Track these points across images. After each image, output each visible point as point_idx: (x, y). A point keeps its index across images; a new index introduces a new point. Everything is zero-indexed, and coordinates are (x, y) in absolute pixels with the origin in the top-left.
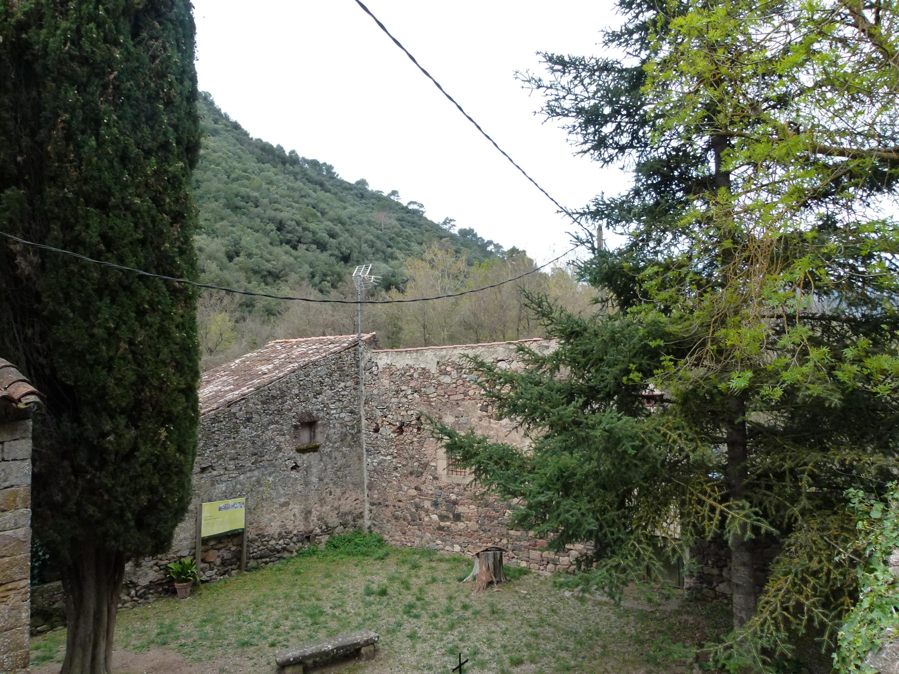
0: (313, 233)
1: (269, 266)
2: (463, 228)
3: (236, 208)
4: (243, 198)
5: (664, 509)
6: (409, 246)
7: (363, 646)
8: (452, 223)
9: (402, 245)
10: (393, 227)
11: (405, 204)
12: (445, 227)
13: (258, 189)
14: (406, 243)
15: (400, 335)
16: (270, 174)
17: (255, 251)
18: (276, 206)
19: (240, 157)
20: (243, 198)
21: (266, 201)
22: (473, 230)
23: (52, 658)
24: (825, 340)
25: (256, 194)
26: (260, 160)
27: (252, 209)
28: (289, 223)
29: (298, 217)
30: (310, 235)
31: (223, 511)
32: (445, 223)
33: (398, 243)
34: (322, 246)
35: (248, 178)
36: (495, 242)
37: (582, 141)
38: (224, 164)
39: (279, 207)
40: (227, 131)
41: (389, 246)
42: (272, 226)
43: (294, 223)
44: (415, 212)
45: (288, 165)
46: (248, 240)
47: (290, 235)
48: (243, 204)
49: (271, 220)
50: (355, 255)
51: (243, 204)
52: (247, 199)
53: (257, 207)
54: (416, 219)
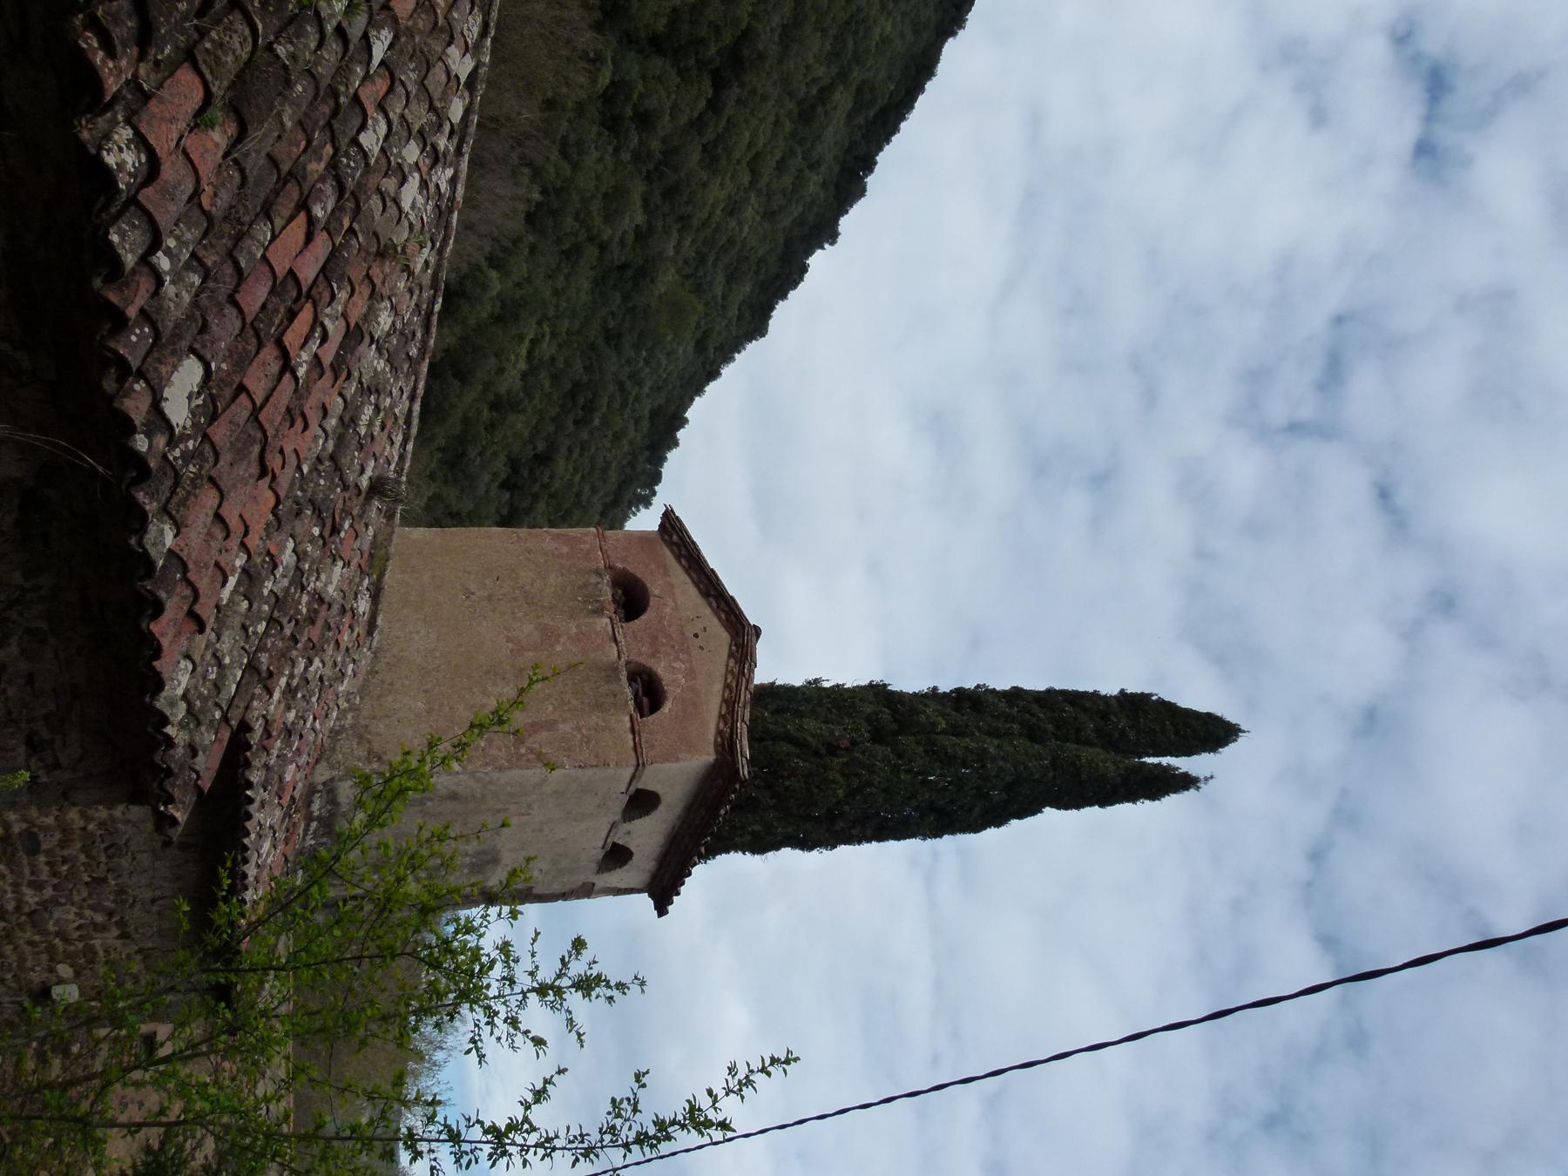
1: (473, 453)
3: (573, 394)
4: (591, 401)
5: (498, 310)
13: (605, 423)
16: (632, 433)
17: (498, 436)
18: (577, 451)
19: (659, 389)
20: (591, 401)
21: (585, 436)
23: (217, 564)
24: (337, 933)
25: (597, 422)
26: (654, 414)
27: (571, 416)
28: (547, 473)
29: (557, 484)
30: (525, 505)
31: (750, 1054)
35: (623, 406)
38: (647, 370)
39: (575, 456)
40: (704, 364)
42: (541, 446)
43: (546, 479)
45: (647, 453)
46: (519, 424)
47: (526, 473)
48: (581, 401)
49: (553, 446)
51: (581, 401)
52: (590, 408)
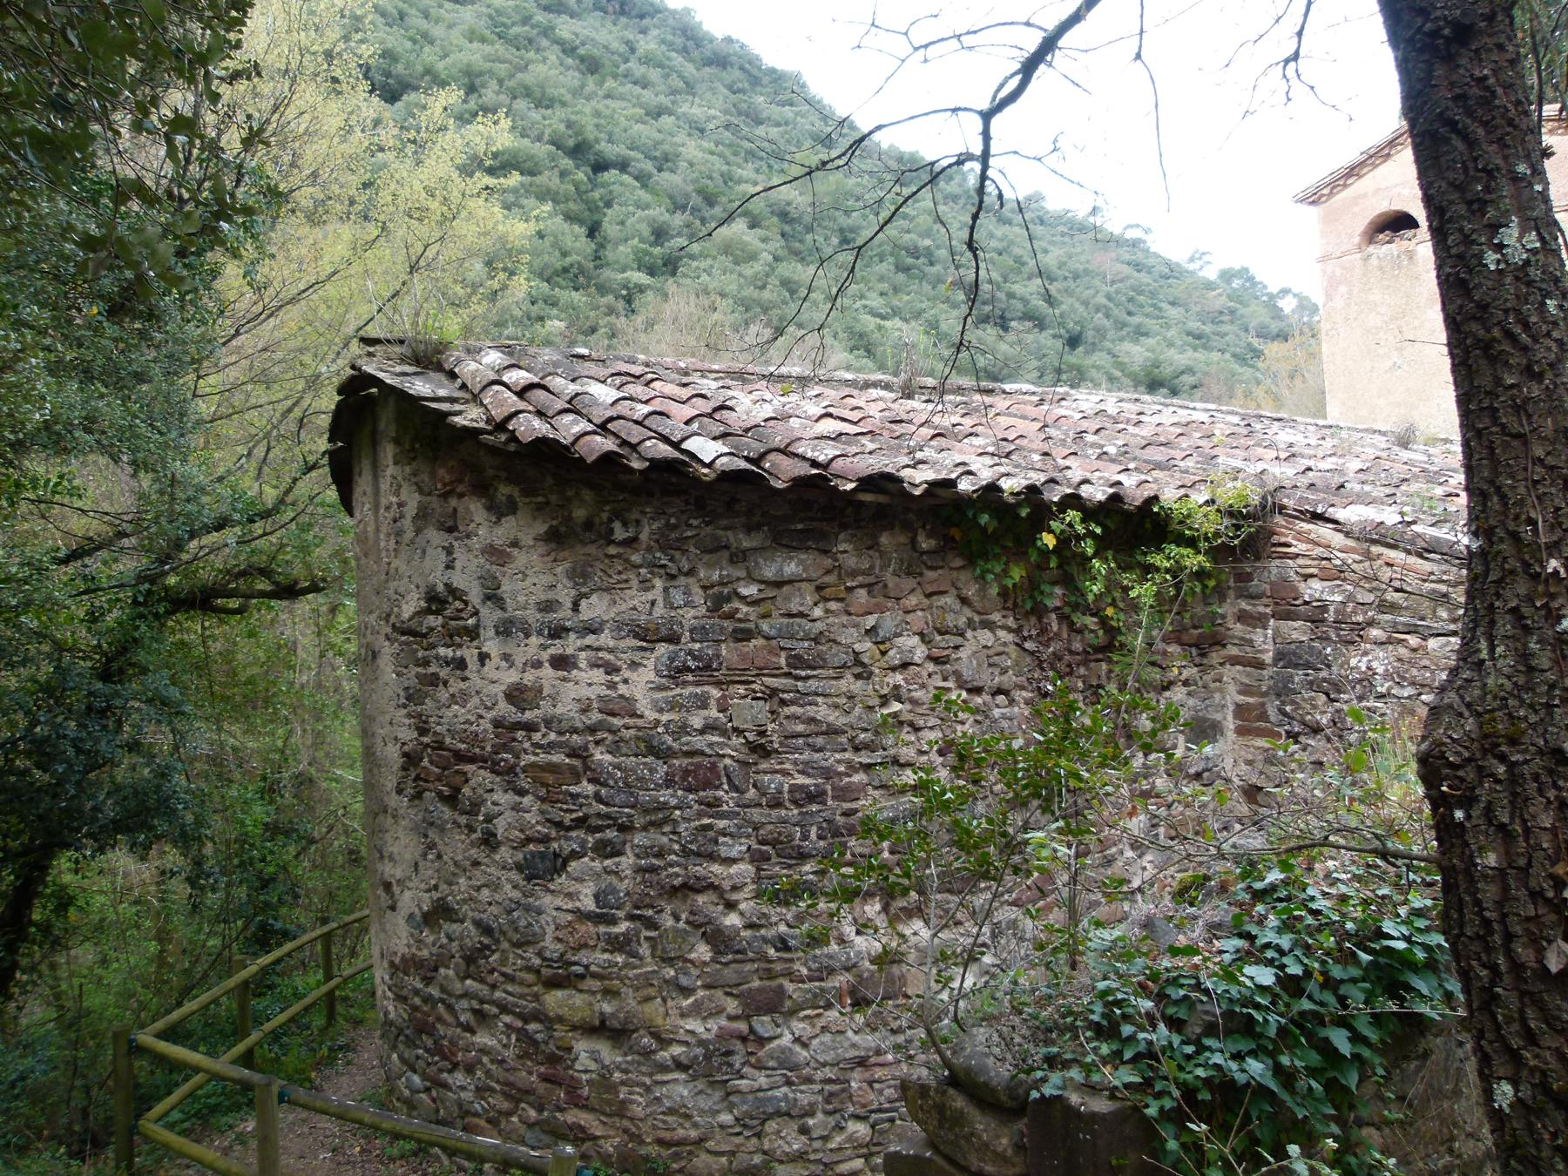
0: (1022, 299)
2: (1227, 266)
6: (1160, 309)
7: (1238, 1031)
8: (1206, 258)
9: (1149, 310)
10: (1128, 278)
11: (1117, 232)
12: (1191, 267)
14: (1154, 305)
15: (423, 604)
22: (1247, 270)
30: (1020, 306)
32: (1192, 260)
33: (1142, 306)
34: (1040, 323)
36: (1295, 290)
37: (768, 333)
41: (1130, 314)
44: (1135, 244)
47: (988, 308)
50: (1090, 335)
53: (932, 264)
54: (1140, 256)
